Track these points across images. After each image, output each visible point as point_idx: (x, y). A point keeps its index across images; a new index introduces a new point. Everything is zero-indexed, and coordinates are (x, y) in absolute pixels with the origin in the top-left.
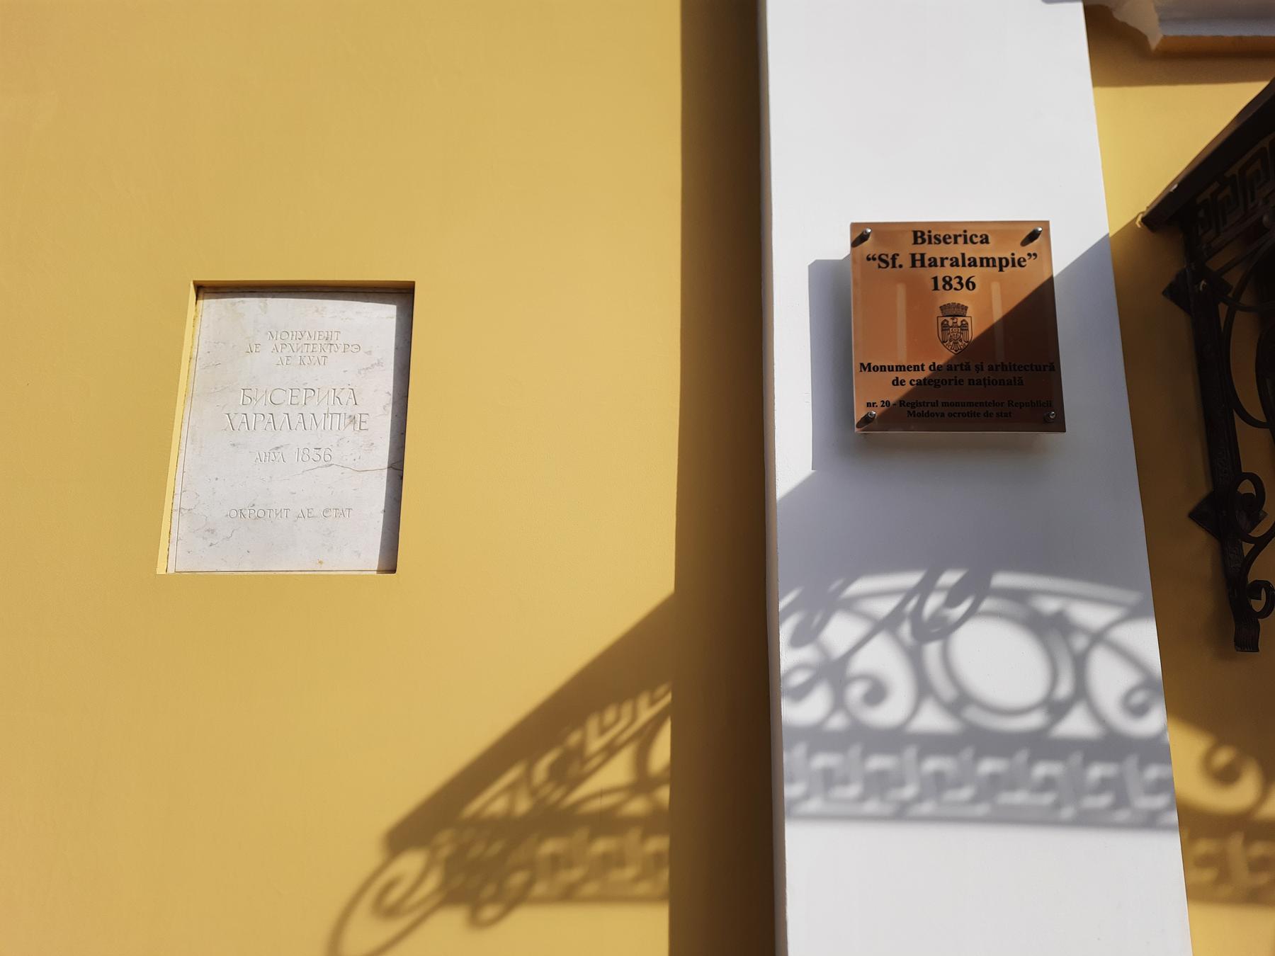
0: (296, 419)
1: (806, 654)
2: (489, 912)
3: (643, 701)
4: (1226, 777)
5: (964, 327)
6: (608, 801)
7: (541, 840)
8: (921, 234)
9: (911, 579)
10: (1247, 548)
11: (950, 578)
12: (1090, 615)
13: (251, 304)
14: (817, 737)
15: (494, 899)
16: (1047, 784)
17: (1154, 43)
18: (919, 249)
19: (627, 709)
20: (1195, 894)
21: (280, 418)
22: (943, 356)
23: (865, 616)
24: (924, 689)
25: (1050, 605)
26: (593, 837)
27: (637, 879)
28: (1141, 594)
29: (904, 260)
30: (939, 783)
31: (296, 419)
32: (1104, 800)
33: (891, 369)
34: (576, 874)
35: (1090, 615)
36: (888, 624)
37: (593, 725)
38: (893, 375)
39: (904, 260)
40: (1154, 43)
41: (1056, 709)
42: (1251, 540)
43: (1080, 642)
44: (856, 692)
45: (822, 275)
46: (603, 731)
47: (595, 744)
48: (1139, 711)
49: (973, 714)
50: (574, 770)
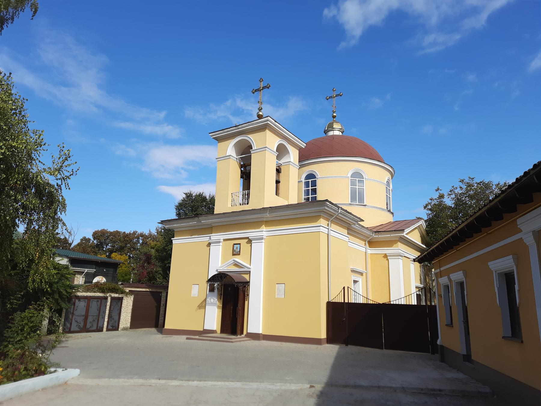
35: (215, 299)
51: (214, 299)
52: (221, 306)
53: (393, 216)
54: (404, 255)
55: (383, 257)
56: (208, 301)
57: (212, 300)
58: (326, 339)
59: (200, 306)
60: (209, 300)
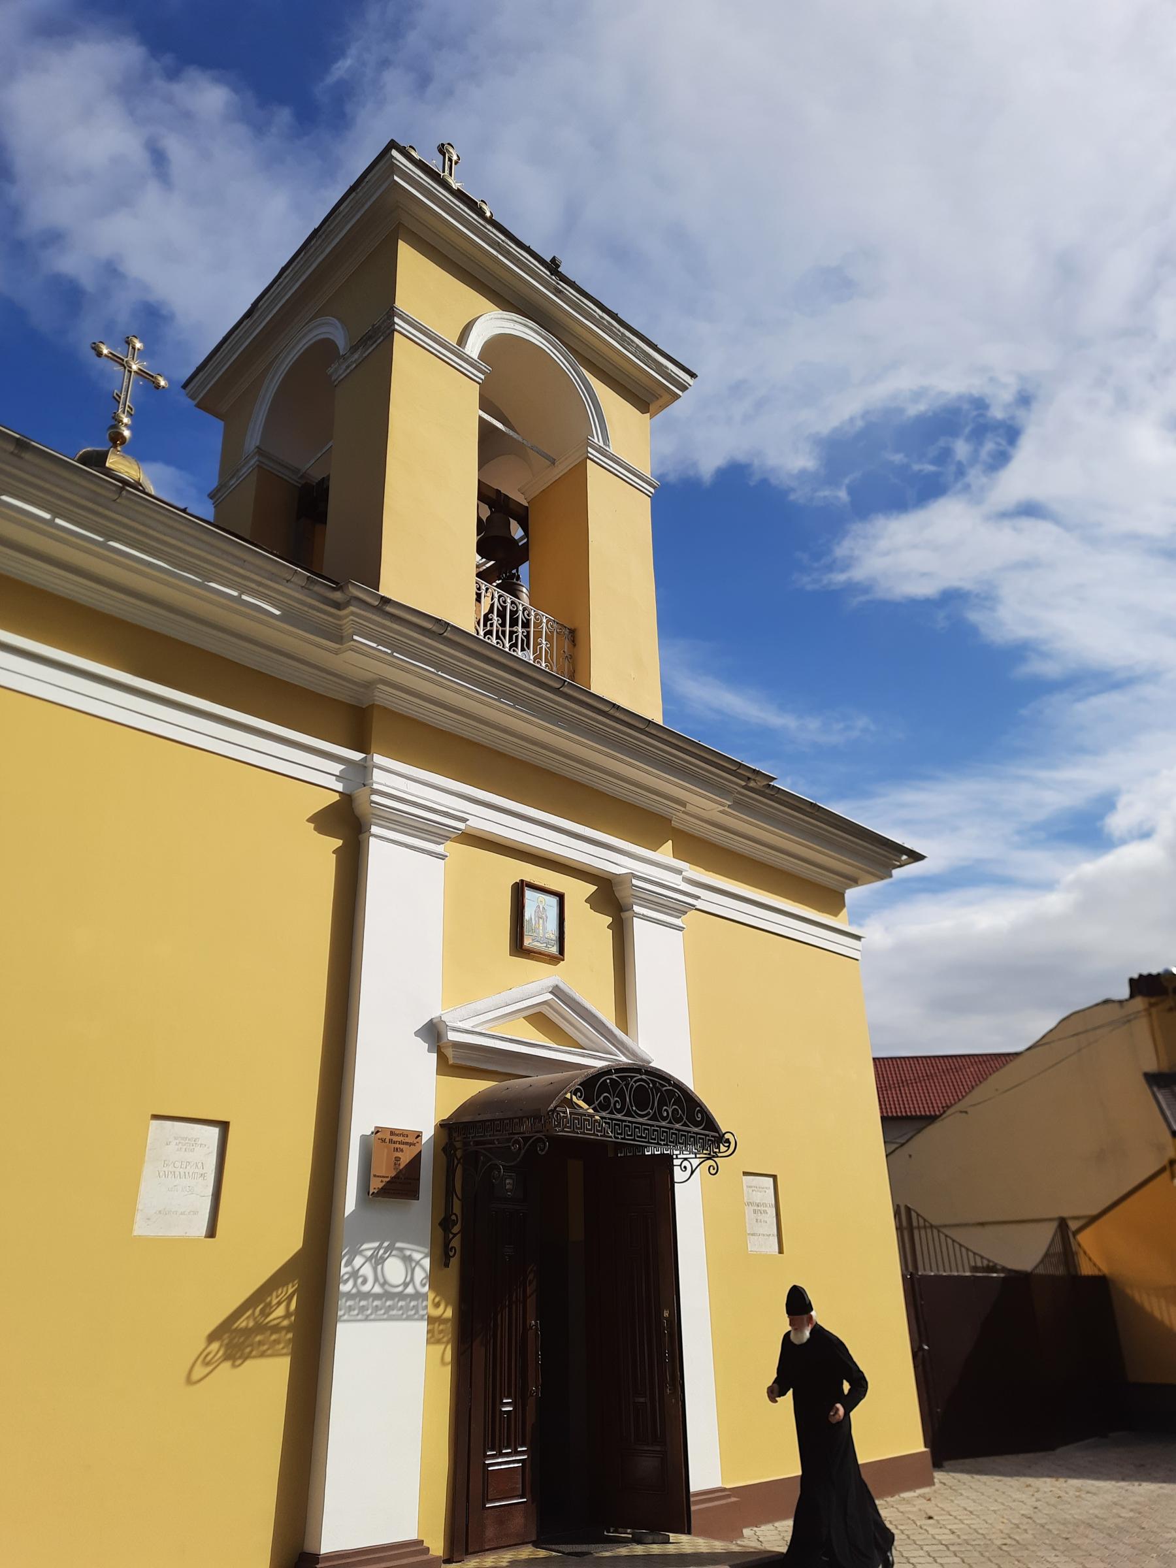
0: (182, 1174)
1: (349, 1269)
2: (238, 1362)
3: (290, 1286)
4: (437, 1305)
5: (399, 1165)
6: (275, 1322)
7: (256, 1335)
8: (393, 1132)
9: (376, 1244)
10: (451, 1236)
11: (386, 1244)
12: (417, 1256)
13: (168, 1123)
14: (349, 1296)
15: (240, 1358)
16: (402, 1307)
17: (451, 1062)
18: (392, 1137)
19: (285, 1289)
20: (428, 1342)
21: (177, 1173)
22: (393, 1174)
23: (364, 1256)
24: (376, 1280)
25: (408, 1253)
26: (272, 1334)
27: (283, 1348)
28: (427, 1250)
29: (387, 1140)
30: (377, 1308)
31: (182, 1174)
32: (413, 1312)
33: (381, 1177)
34: (265, 1347)
35: (417, 1256)
36: (369, 1259)
37: (274, 1294)
38: (381, 1179)
39: (387, 1140)
40: (451, 1062)
41: (406, 1285)
42: (452, 1233)
43: (413, 1264)
44: (360, 1280)
45: (364, 1139)
46: (277, 1297)
47: (275, 1302)
48: (424, 1285)
49: (387, 1287)
50: (267, 1311)
51: (407, 1260)
52: (449, 1313)
53: (415, 150)
54: (464, 820)
55: (310, 820)
56: (355, 1274)
57: (394, 1270)
58: (800, 1478)
59: (242, 1323)
60: (367, 1270)
